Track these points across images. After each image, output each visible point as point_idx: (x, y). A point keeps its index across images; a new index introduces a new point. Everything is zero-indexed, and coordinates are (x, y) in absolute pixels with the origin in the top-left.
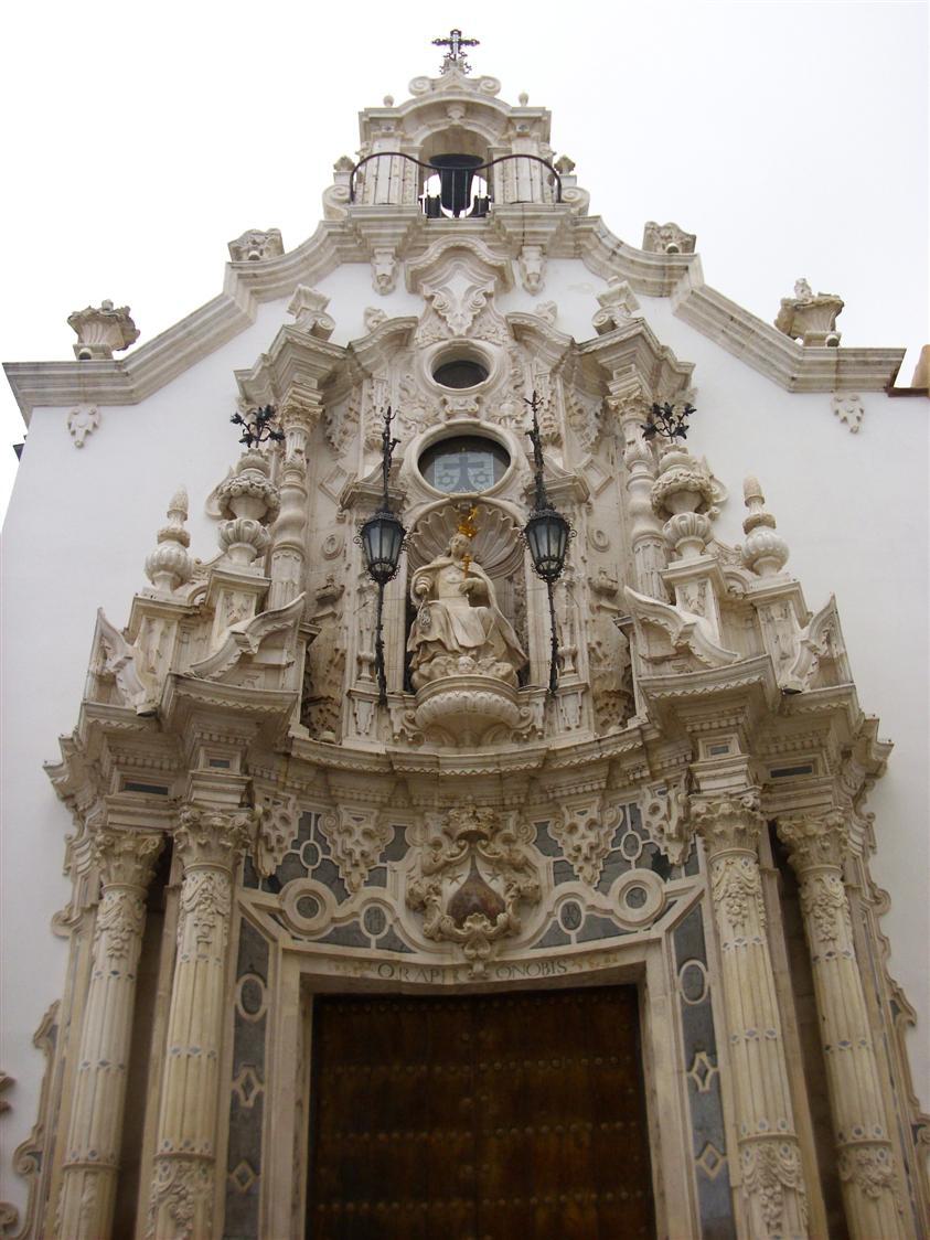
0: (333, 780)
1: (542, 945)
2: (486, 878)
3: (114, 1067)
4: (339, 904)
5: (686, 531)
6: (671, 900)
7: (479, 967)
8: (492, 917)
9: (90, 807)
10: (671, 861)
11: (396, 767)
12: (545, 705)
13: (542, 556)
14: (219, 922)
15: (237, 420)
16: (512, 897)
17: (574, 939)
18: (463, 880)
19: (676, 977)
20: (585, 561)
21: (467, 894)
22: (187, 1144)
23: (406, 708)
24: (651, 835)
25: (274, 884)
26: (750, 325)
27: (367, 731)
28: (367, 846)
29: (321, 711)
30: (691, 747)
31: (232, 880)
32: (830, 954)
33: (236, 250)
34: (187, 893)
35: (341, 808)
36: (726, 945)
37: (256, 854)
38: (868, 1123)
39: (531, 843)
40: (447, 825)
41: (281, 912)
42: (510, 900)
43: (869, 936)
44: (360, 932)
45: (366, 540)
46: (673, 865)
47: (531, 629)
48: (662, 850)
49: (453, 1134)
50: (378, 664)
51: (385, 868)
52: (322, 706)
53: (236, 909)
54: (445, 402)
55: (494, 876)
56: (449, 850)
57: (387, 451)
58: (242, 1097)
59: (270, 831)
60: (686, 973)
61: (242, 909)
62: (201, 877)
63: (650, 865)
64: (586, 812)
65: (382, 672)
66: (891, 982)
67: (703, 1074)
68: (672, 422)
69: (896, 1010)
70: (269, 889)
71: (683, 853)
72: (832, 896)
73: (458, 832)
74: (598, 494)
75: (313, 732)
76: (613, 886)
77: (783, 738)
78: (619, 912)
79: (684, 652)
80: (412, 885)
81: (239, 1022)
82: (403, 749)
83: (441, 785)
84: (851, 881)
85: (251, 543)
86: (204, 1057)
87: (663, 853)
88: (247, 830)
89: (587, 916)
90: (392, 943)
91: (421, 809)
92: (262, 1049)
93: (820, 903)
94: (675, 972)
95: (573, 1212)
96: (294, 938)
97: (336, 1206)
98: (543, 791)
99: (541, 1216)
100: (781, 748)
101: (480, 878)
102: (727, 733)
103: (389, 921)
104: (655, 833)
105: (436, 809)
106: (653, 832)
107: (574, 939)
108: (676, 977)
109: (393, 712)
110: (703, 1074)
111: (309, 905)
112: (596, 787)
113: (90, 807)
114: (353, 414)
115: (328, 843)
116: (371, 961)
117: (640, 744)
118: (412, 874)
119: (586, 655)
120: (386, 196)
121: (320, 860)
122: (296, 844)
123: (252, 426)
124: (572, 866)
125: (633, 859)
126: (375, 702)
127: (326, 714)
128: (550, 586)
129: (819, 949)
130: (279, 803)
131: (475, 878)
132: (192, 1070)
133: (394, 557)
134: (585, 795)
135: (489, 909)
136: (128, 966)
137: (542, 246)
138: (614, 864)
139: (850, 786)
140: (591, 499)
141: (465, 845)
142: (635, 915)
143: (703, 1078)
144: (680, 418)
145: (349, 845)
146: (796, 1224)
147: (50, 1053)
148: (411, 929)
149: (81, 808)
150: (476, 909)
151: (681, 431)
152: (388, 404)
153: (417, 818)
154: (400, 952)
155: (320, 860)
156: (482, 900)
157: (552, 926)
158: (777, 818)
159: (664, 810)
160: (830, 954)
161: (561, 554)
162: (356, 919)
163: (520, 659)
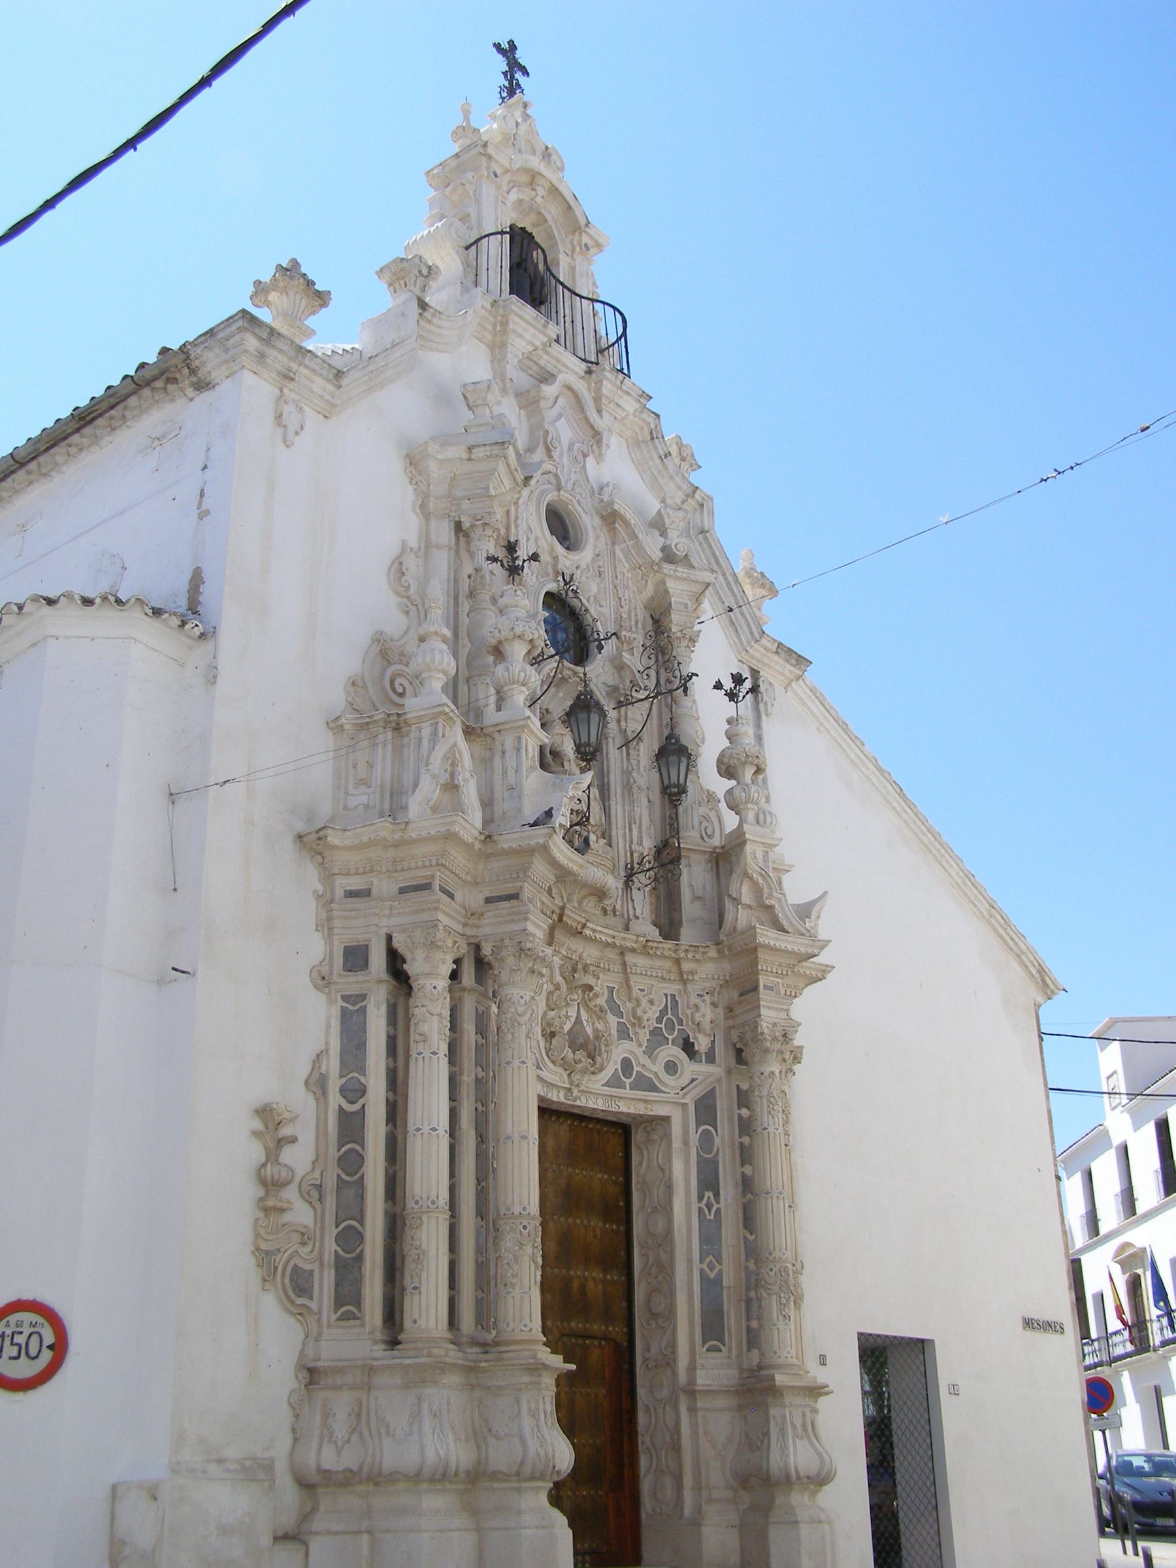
33: (329, 292)
36: (755, 1131)
58: (712, 1197)
67: (709, 1206)
87: (691, 1040)
95: (591, 1284)
99: (576, 1284)
110: (709, 1206)
125: (670, 1038)
156: (585, 1040)
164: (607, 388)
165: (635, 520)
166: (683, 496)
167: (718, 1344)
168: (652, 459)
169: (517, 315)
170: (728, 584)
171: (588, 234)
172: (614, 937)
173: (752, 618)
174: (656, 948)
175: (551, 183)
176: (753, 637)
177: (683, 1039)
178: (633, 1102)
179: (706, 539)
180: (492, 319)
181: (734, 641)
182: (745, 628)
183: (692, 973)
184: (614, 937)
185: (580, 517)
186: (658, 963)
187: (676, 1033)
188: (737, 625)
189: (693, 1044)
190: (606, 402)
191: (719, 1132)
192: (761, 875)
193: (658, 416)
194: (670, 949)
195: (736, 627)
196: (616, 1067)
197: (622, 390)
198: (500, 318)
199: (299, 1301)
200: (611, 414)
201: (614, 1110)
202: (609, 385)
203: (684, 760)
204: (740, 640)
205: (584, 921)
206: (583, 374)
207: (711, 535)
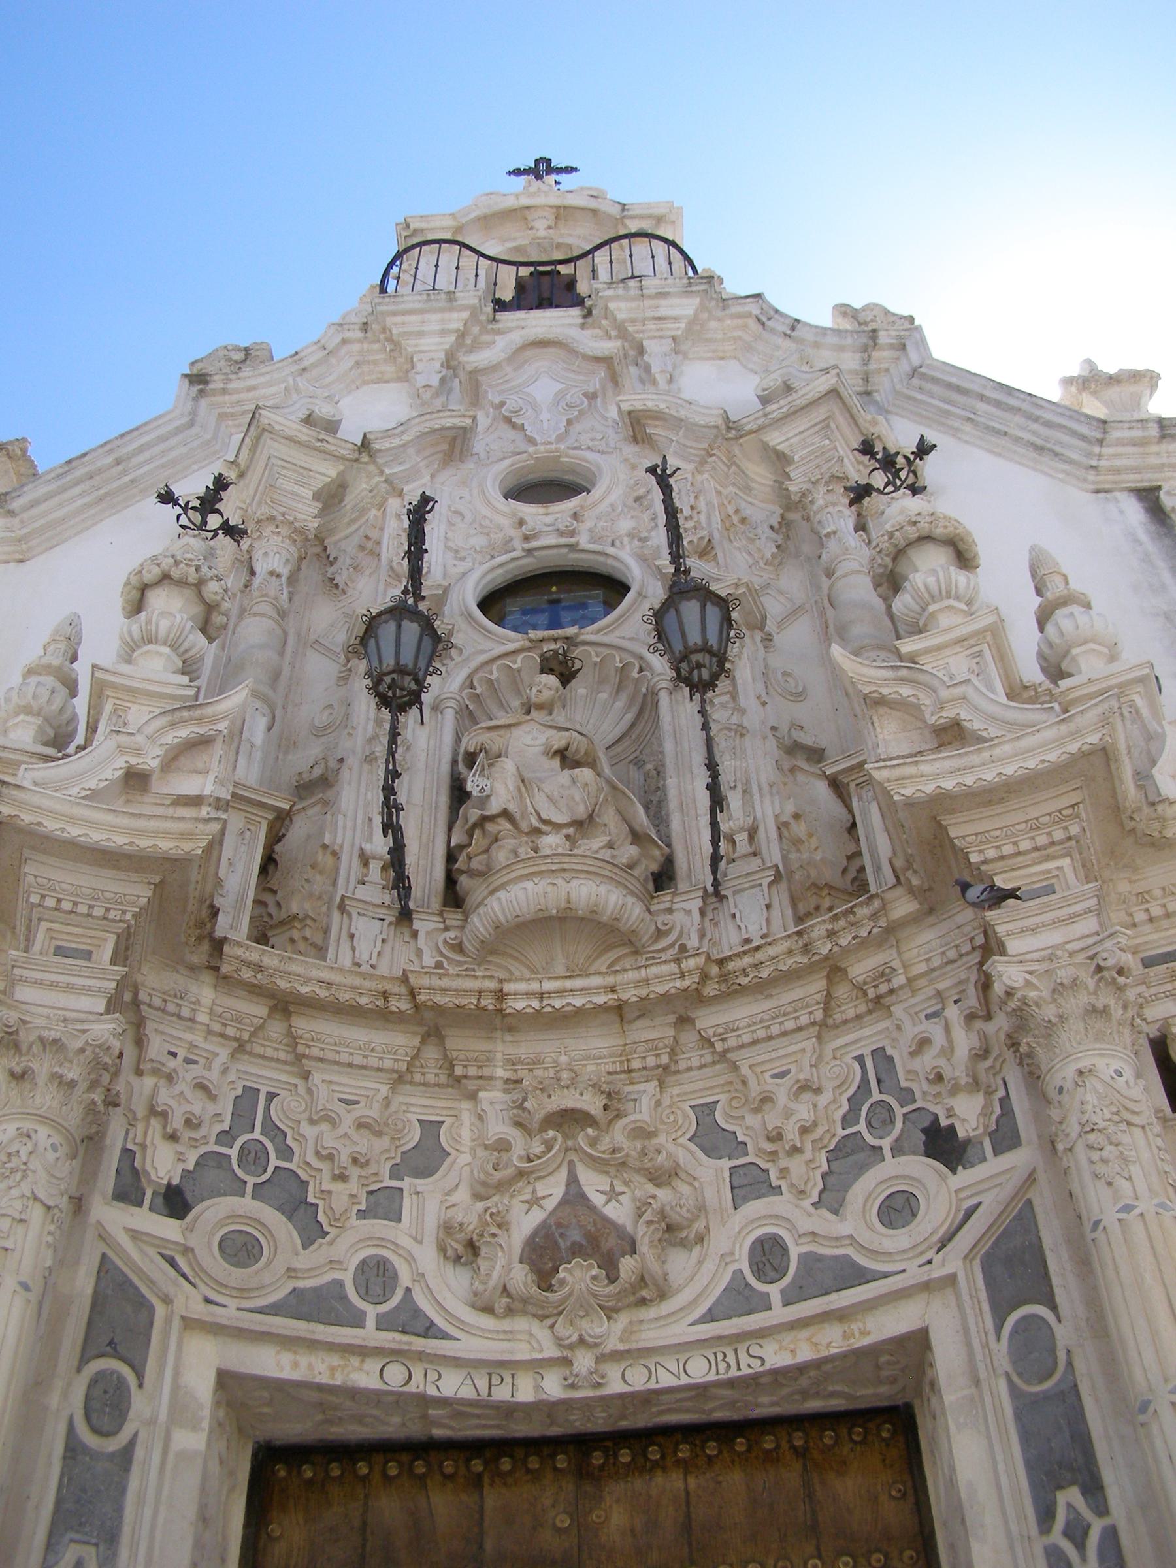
0: (303, 1025)
2: (597, 1199)
4: (305, 1247)
5: (936, 593)
10: (961, 1134)
12: (702, 912)
13: (691, 643)
14: (36, 1213)
16: (650, 1223)
18: (550, 1204)
19: (993, 1344)
20: (764, 704)
21: (559, 1225)
23: (447, 929)
24: (918, 1095)
26: (1012, 402)
27: (374, 961)
28: (363, 1143)
35: (317, 1077)
36: (1097, 1223)
41: (187, 1250)
44: (344, 1298)
46: (968, 1141)
51: (401, 1190)
52: (296, 934)
55: (612, 1195)
59: (171, 1102)
60: (1015, 1331)
64: (788, 1072)
67: (1077, 1533)
70: (165, 1212)
71: (985, 1112)
73: (539, 1116)
74: (781, 625)
76: (850, 1196)
77: (1158, 893)
81: (73, 1449)
85: (171, 647)
87: (944, 1122)
89: (803, 1258)
91: (471, 1085)
92: (119, 1510)
94: (992, 1337)
96: (207, 1301)
98: (707, 1042)
100: (1156, 911)
101: (584, 1197)
102: (1049, 858)
104: (925, 1086)
105: (499, 1084)
108: (993, 1344)
109: (421, 936)
110: (1077, 1533)
112: (804, 1020)
114: (370, 545)
116: (363, 1352)
118: (454, 1198)
119: (774, 834)
120: (517, 1382)
121: (270, 1170)
122: (226, 1137)
124: (767, 1171)
126: (389, 919)
130: (195, 1062)
131: (575, 1197)
134: (784, 1040)
140: (770, 626)
141: (555, 1139)
142: (898, 1239)
143: (1081, 1546)
150: (576, 1251)
153: (466, 1105)
154: (425, 1336)
155: (270, 1170)
157: (733, 1279)
162: (337, 1275)
163: (657, 853)
164: (622, 309)
165: (665, 401)
166: (858, 356)
168: (777, 348)
169: (394, 314)
170: (998, 404)
171: (632, 217)
172: (613, 989)
173: (1071, 417)
174: (755, 966)
175: (551, 207)
177: (924, 1131)
178: (804, 1334)
179: (923, 376)
180: (376, 346)
181: (1064, 471)
182: (1067, 439)
183: (884, 974)
184: (613, 989)
185: (587, 461)
186: (788, 996)
187: (899, 1125)
188: (1049, 446)
189: (952, 1129)
190: (639, 327)
192: (902, 680)
193: (758, 296)
194: (790, 952)
195: (1049, 450)
196: (736, 1266)
197: (650, 297)
198: (382, 336)
200: (661, 337)
201: (746, 1371)
202: (622, 305)
204: (1071, 462)
205: (491, 985)
206: (581, 321)
207: (928, 366)
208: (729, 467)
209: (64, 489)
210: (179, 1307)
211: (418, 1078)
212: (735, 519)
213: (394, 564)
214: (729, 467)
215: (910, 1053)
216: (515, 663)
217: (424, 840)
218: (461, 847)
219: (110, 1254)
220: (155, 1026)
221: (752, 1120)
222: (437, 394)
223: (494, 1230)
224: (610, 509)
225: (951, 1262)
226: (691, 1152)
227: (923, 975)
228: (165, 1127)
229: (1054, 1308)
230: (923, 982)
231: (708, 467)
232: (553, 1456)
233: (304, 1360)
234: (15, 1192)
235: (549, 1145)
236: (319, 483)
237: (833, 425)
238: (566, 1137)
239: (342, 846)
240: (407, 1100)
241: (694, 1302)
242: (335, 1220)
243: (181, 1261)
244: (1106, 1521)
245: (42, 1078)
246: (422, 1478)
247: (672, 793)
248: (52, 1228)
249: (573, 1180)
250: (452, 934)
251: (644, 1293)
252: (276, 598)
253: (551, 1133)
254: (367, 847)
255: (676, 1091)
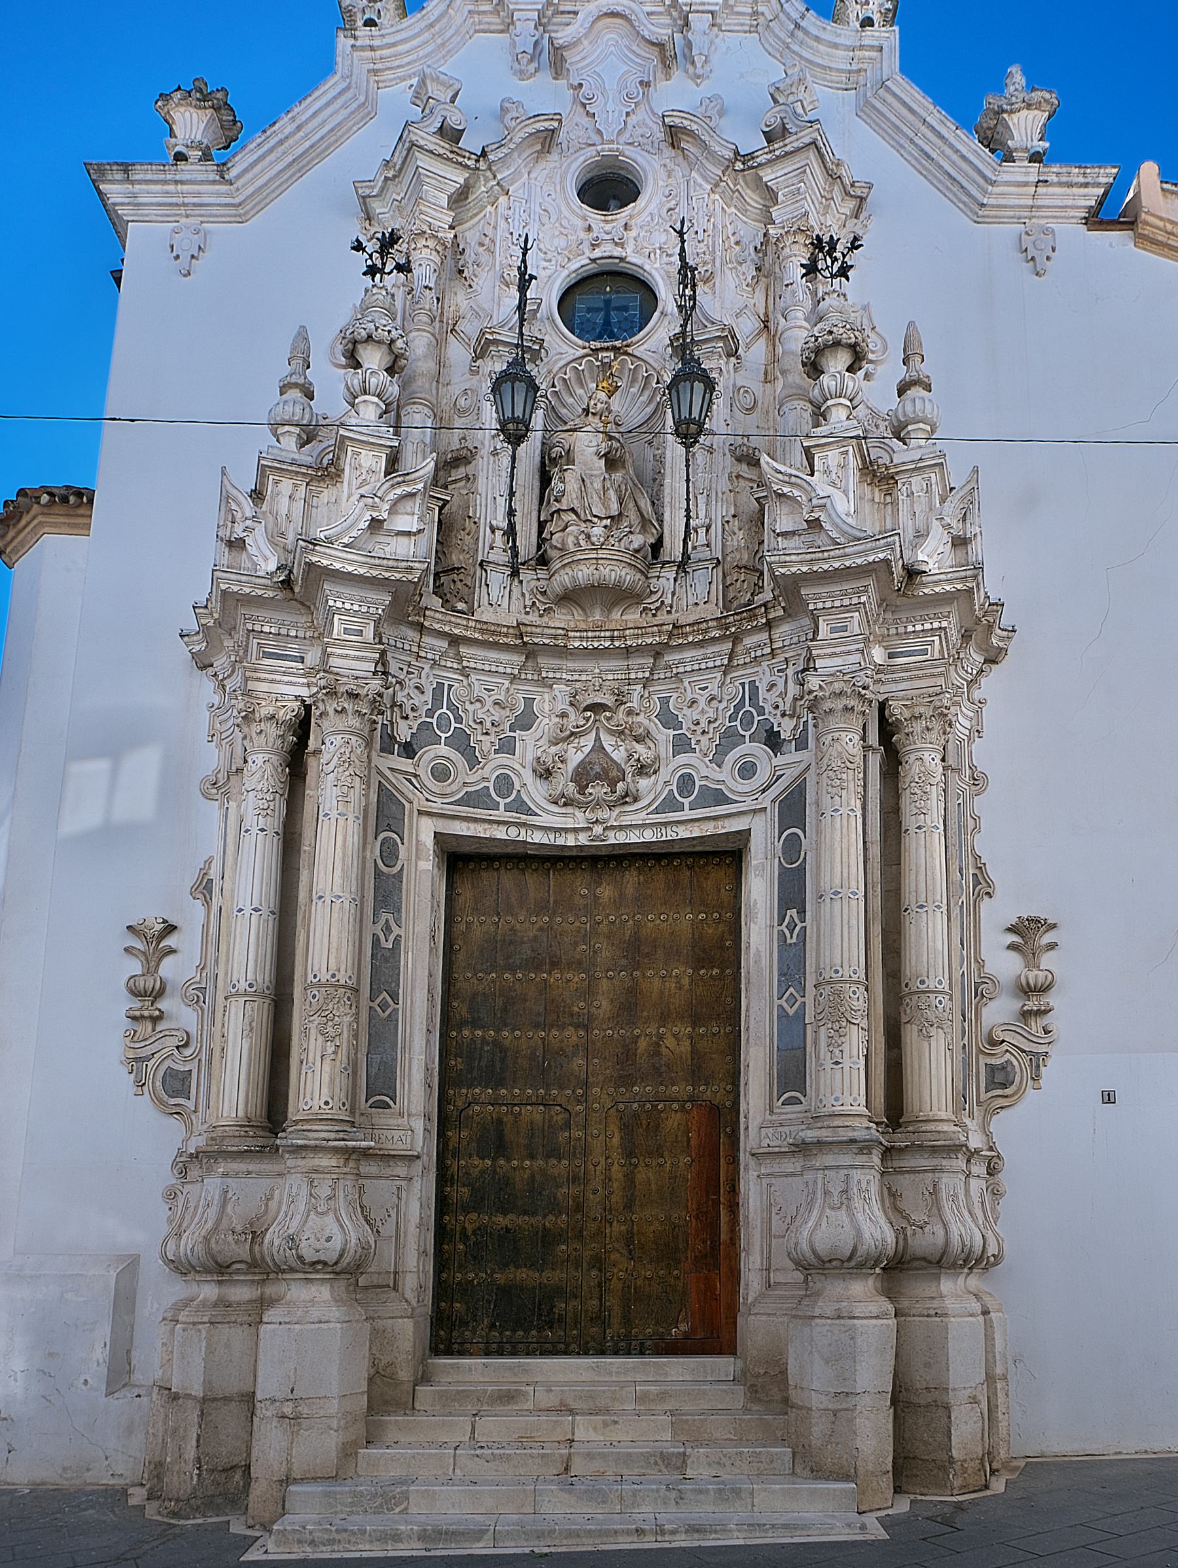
1: (657, 811)
2: (609, 749)
3: (265, 911)
6: (778, 773)
7: (598, 829)
8: (613, 784)
9: (229, 676)
11: (525, 639)
12: (675, 580)
15: (358, 247)
17: (687, 807)
18: (587, 750)
21: (590, 763)
22: (333, 976)
24: (766, 711)
25: (409, 750)
28: (498, 714)
29: (454, 581)
30: (813, 626)
31: (369, 744)
32: (919, 828)
34: (328, 752)
37: (391, 722)
38: (931, 974)
39: (653, 717)
40: (574, 697)
41: (416, 776)
42: (630, 769)
43: (961, 814)
45: (498, 397)
47: (667, 499)
48: (775, 726)
49: (569, 976)
50: (511, 532)
53: (374, 771)
54: (589, 229)
56: (574, 719)
57: (523, 286)
61: (380, 773)
62: (338, 740)
63: (763, 741)
64: (707, 687)
65: (514, 541)
66: (977, 858)
67: (792, 927)
68: (835, 260)
69: (977, 883)
72: (929, 774)
75: (446, 602)
78: (730, 783)
79: (815, 525)
80: (539, 754)
81: (378, 874)
82: (533, 618)
83: (569, 657)
84: (951, 761)
85: (378, 396)
86: (346, 904)
88: (382, 697)
90: (520, 806)
93: (917, 780)
94: (776, 839)
96: (427, 800)
97: (466, 1032)
102: (849, 611)
103: (517, 786)
106: (768, 708)
107: (687, 807)
110: (792, 927)
111: (441, 774)
112: (718, 663)
113: (229, 676)
114: (487, 241)
115: (460, 713)
117: (764, 621)
118: (540, 743)
121: (452, 729)
122: (430, 713)
123: (375, 255)
125: (747, 734)
127: (459, 585)
128: (687, 452)
129: (909, 821)
131: (599, 747)
132: (335, 916)
133: (527, 416)
135: (610, 775)
136: (274, 823)
137: (712, 12)
138: (730, 739)
139: (966, 671)
142: (744, 786)
144: (844, 256)
145: (480, 715)
146: (855, 1053)
147: (207, 903)
148: (535, 792)
149: (221, 677)
150: (598, 777)
151: (844, 272)
152: (526, 230)
153: (546, 690)
155: (452, 729)
156: (603, 769)
158: (887, 699)
159: (780, 687)
160: (919, 828)
161: (703, 418)
162: (486, 784)
167: (798, 1095)
176: (987, 182)
178: (697, 824)
191: (405, 841)
199: (173, 1101)
203: (699, 387)
208: (734, 192)
209: (262, 158)
210: (416, 806)
211: (523, 676)
212: (733, 239)
213: (505, 275)
214: (734, 192)
215: (767, 690)
216: (580, 365)
217: (525, 512)
218: (546, 522)
219: (382, 781)
220: (392, 655)
221: (686, 711)
222: (531, 60)
223: (560, 765)
224: (649, 218)
225: (766, 800)
226: (656, 724)
227: (780, 648)
228: (401, 712)
229: (805, 833)
230: (779, 651)
231: (719, 190)
232: (581, 863)
233: (472, 826)
234: (347, 773)
235: (588, 719)
236: (452, 188)
237: (808, 171)
238: (595, 714)
239: (479, 519)
240: (518, 687)
241: (649, 805)
242: (484, 756)
243: (414, 780)
244: (804, 924)
245: (350, 712)
246: (523, 870)
247: (667, 491)
248: (364, 787)
249: (598, 738)
250: (542, 582)
251: (627, 799)
252: (430, 310)
253: (589, 713)
254: (494, 523)
255: (651, 689)
